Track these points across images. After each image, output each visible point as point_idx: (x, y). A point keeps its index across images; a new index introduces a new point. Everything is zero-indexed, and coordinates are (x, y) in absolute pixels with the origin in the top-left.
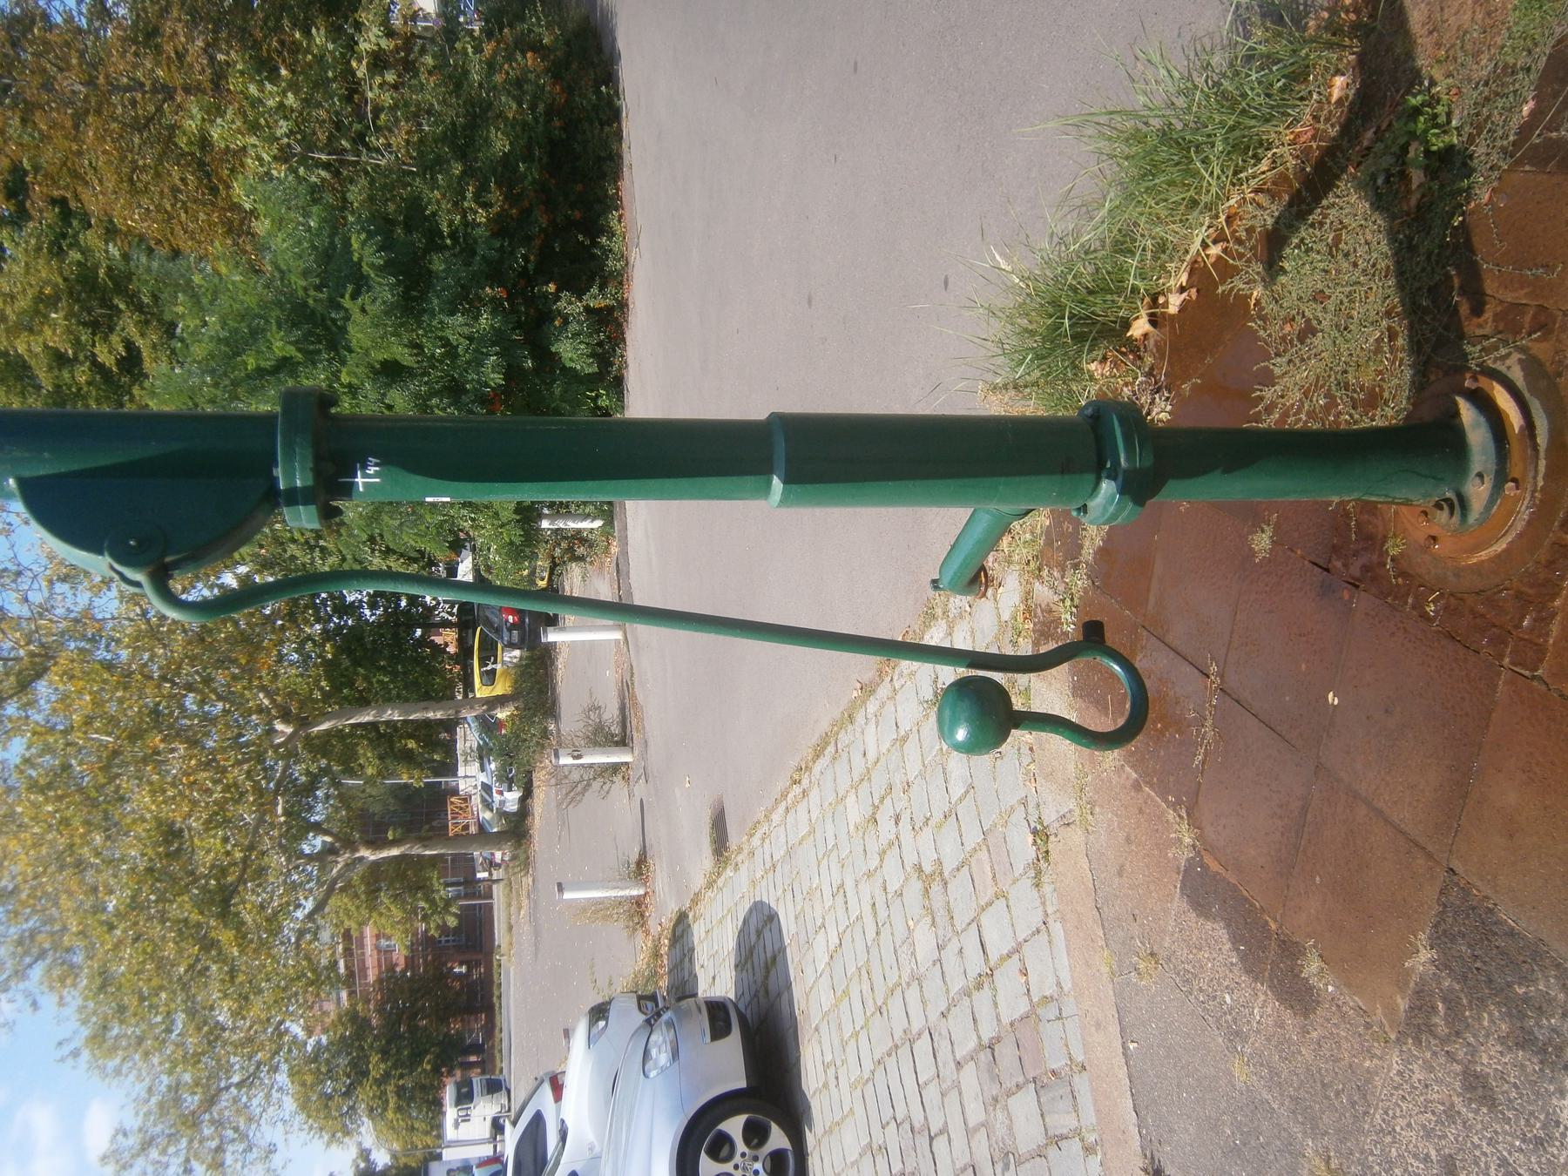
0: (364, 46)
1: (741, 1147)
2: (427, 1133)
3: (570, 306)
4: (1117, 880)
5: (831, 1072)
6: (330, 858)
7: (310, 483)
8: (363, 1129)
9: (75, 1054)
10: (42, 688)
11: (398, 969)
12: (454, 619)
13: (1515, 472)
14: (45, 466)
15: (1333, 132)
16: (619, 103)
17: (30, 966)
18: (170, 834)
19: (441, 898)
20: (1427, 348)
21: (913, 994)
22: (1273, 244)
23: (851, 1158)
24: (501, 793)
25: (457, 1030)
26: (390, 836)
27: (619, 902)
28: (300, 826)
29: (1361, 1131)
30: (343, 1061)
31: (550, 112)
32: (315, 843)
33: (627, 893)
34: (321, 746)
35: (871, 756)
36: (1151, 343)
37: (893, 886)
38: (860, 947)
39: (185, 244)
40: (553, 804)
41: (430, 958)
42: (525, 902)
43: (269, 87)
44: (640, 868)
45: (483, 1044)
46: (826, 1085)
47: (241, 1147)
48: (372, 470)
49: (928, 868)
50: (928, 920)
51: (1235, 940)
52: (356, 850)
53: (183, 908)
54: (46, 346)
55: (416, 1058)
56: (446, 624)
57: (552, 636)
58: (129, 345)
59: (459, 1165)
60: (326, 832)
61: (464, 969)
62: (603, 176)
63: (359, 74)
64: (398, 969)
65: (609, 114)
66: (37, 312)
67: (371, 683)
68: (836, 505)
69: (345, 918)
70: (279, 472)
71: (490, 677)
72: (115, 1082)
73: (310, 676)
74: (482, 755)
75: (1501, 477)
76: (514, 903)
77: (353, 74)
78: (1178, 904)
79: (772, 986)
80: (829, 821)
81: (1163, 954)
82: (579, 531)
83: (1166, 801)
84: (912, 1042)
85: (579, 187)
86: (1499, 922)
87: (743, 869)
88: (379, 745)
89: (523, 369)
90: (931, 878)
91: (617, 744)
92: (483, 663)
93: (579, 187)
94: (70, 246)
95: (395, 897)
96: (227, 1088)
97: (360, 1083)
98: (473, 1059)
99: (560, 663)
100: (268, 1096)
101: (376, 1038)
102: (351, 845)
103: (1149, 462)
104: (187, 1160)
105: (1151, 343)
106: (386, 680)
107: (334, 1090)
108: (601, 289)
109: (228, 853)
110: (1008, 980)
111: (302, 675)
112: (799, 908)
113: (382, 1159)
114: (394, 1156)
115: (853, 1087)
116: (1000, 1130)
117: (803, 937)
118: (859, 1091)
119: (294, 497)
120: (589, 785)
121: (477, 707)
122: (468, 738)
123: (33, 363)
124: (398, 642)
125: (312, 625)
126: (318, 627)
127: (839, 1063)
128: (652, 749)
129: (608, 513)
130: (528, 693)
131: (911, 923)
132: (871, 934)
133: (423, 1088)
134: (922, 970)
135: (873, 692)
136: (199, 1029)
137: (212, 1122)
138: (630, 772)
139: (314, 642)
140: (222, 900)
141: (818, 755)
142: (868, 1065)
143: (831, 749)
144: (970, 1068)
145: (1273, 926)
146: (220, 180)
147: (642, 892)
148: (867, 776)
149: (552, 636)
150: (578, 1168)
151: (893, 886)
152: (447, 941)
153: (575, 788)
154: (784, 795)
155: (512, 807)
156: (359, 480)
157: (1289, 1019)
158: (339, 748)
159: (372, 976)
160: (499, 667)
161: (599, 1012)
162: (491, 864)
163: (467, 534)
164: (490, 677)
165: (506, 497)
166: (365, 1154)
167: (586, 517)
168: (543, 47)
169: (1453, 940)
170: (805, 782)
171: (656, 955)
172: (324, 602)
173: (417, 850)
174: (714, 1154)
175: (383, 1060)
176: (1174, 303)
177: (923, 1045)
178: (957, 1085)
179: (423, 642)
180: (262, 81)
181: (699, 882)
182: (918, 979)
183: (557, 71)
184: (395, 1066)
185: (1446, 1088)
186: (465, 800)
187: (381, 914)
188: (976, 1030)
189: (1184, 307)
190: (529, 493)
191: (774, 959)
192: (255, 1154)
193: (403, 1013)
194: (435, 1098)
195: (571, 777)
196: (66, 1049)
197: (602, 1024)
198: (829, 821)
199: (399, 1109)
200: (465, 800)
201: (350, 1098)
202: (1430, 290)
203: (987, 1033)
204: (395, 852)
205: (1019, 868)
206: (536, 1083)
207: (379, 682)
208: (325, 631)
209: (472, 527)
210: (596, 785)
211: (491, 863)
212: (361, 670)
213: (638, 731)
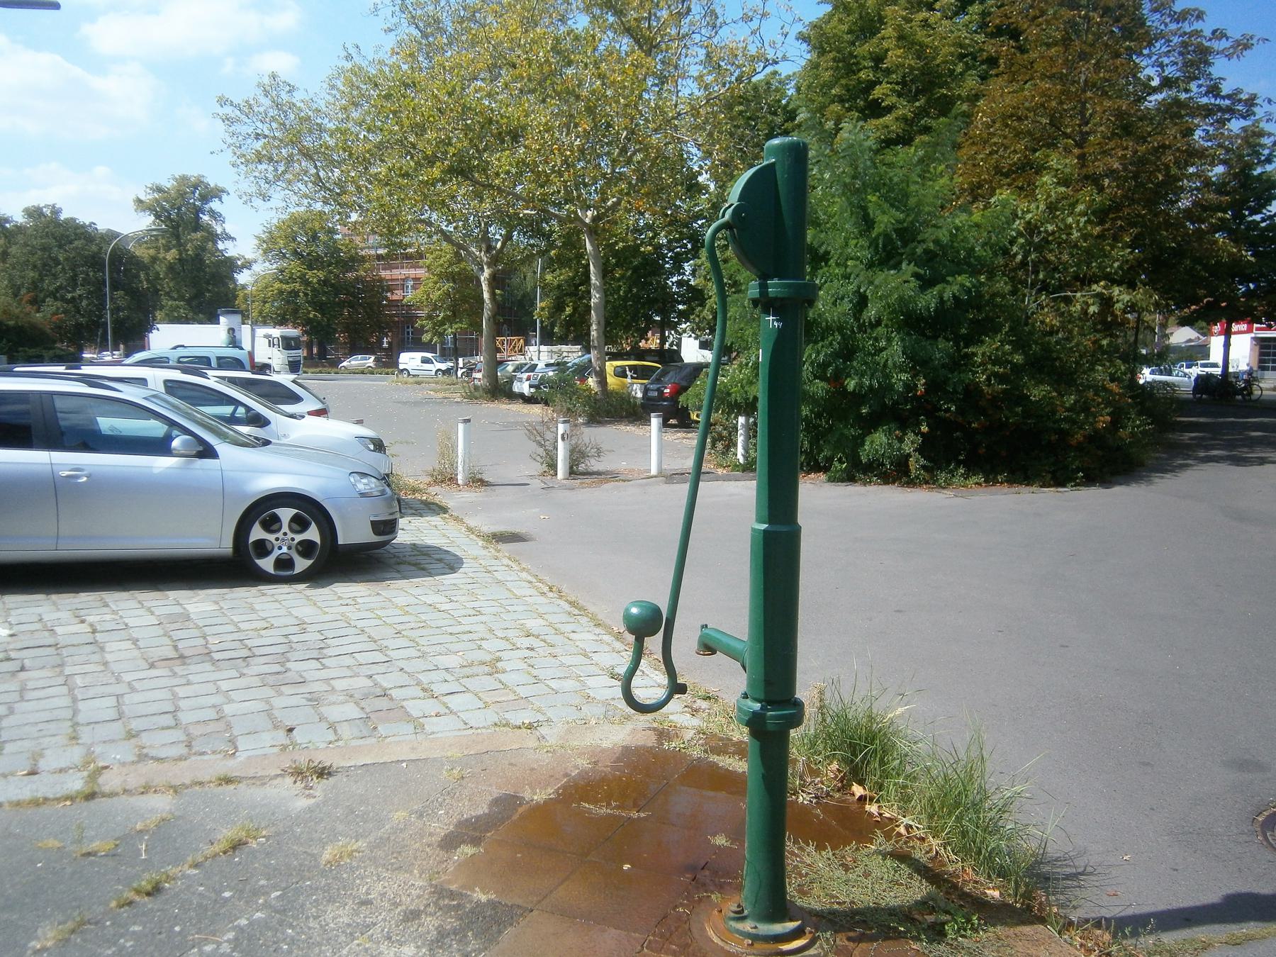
0: (1116, 291)
1: (299, 538)
2: (261, 313)
3: (910, 444)
4: (507, 762)
5: (349, 601)
6: (484, 246)
7: (770, 295)
8: (267, 264)
9: (349, 57)
10: (625, 43)
11: (389, 294)
12: (667, 346)
13: (758, 945)
14: (781, 175)
15: (966, 889)
16: (1068, 485)
17: (417, 27)
18: (516, 136)
19: (445, 330)
20: (831, 917)
21: (413, 652)
22: (902, 857)
23: (294, 612)
24: (528, 379)
25: (338, 338)
26: (498, 292)
27: (453, 465)
28: (510, 222)
29: (377, 867)
30: (321, 250)
31: (1063, 434)
32: (496, 233)
33: (460, 468)
34: (571, 241)
35: (572, 636)
36: (848, 797)
37: (484, 644)
38: (440, 623)
39: (965, 152)
40: (520, 419)
41: (396, 319)
42: (440, 395)
43: (1083, 220)
44: (478, 482)
45: (326, 359)
46: (340, 598)
47: (270, 177)
48: (776, 324)
49: (499, 665)
50: (465, 664)
51: (478, 818)
52: (489, 265)
53: (459, 142)
54: (887, 50)
55: (320, 307)
56: (663, 340)
57: (655, 421)
58: (889, 109)
59: (238, 337)
60: (504, 244)
61: (385, 345)
62: (1012, 472)
63: (1094, 287)
64: (389, 294)
65: (1059, 479)
66: (913, 43)
67: (619, 280)
68: (750, 621)
69: (434, 256)
70: (776, 281)
71: (621, 373)
72: (325, 86)
73: (627, 234)
74: (560, 366)
75: (756, 938)
76: (439, 387)
77: (1097, 282)
78: (496, 793)
79: (403, 567)
80: (526, 608)
81: (464, 783)
82: (735, 445)
83: (559, 788)
84: (380, 650)
85: (1004, 453)
86: (505, 928)
87: (485, 552)
88: (569, 285)
89: (861, 406)
90: (493, 666)
91: (571, 468)
92: (632, 368)
93: (1004, 453)
94: (966, 63)
95: (448, 294)
96: (316, 167)
97: (303, 263)
98: (315, 350)
99: (631, 428)
100: (306, 196)
101: (337, 276)
102: (494, 262)
103: (770, 728)
104: (265, 137)
105: (848, 797)
106: (621, 293)
107: (299, 243)
108: (924, 467)
109: (497, 174)
110: (430, 706)
111: (628, 229)
112: (462, 586)
113: (243, 278)
114: (244, 287)
115: (343, 614)
116: (332, 698)
117: (442, 588)
118: (340, 618)
119: (763, 287)
120: (541, 446)
121: (599, 362)
122: (572, 354)
123: (875, 40)
124: (651, 302)
125: (666, 237)
126: (665, 241)
127: (357, 606)
128: (567, 493)
129: (748, 467)
130: (608, 403)
131: (461, 653)
132: (450, 630)
133: (295, 311)
134: (430, 659)
135: (617, 639)
136: (368, 152)
137: (291, 155)
138: (549, 477)
139: (653, 238)
140: (461, 170)
141: (572, 603)
142: (360, 624)
143: (576, 612)
144: (369, 683)
145: (489, 834)
146: (1014, 180)
147: (460, 482)
148: (558, 632)
149: (655, 421)
150: (272, 426)
151: (484, 644)
152: (408, 333)
153: (538, 434)
154: (540, 581)
155: (517, 387)
156: (771, 318)
157: (434, 839)
158: (570, 254)
159: (385, 274)
160: (629, 380)
161: (379, 446)
162: (470, 370)
163: (735, 359)
164: (621, 373)
165: (760, 390)
166: (248, 265)
167: (746, 450)
168: (1117, 430)
169: (493, 909)
170: (551, 595)
171: (414, 491)
172: (685, 246)
173: (486, 313)
174: (295, 519)
175: (319, 281)
176: (873, 808)
177: (379, 657)
178: (356, 675)
179: (649, 320)
180: (1087, 214)
181: (472, 522)
182: (423, 656)
183: (1096, 438)
184: (314, 290)
185: (409, 903)
186: (520, 351)
187: (436, 283)
188: (395, 687)
189: (871, 814)
190: (762, 405)
191: (423, 569)
192: (264, 186)
193: (354, 297)
194: (287, 320)
195: (548, 433)
196: (352, 51)
197: (372, 447)
198: (526, 608)
199: (281, 292)
200: (520, 351)
201: (292, 255)
202: (864, 921)
203: (394, 693)
204: (486, 296)
205: (507, 716)
206: (322, 398)
207: (620, 286)
208: (660, 246)
209: (741, 362)
210: (541, 451)
211: (472, 369)
212: (629, 273)
213: (581, 483)
